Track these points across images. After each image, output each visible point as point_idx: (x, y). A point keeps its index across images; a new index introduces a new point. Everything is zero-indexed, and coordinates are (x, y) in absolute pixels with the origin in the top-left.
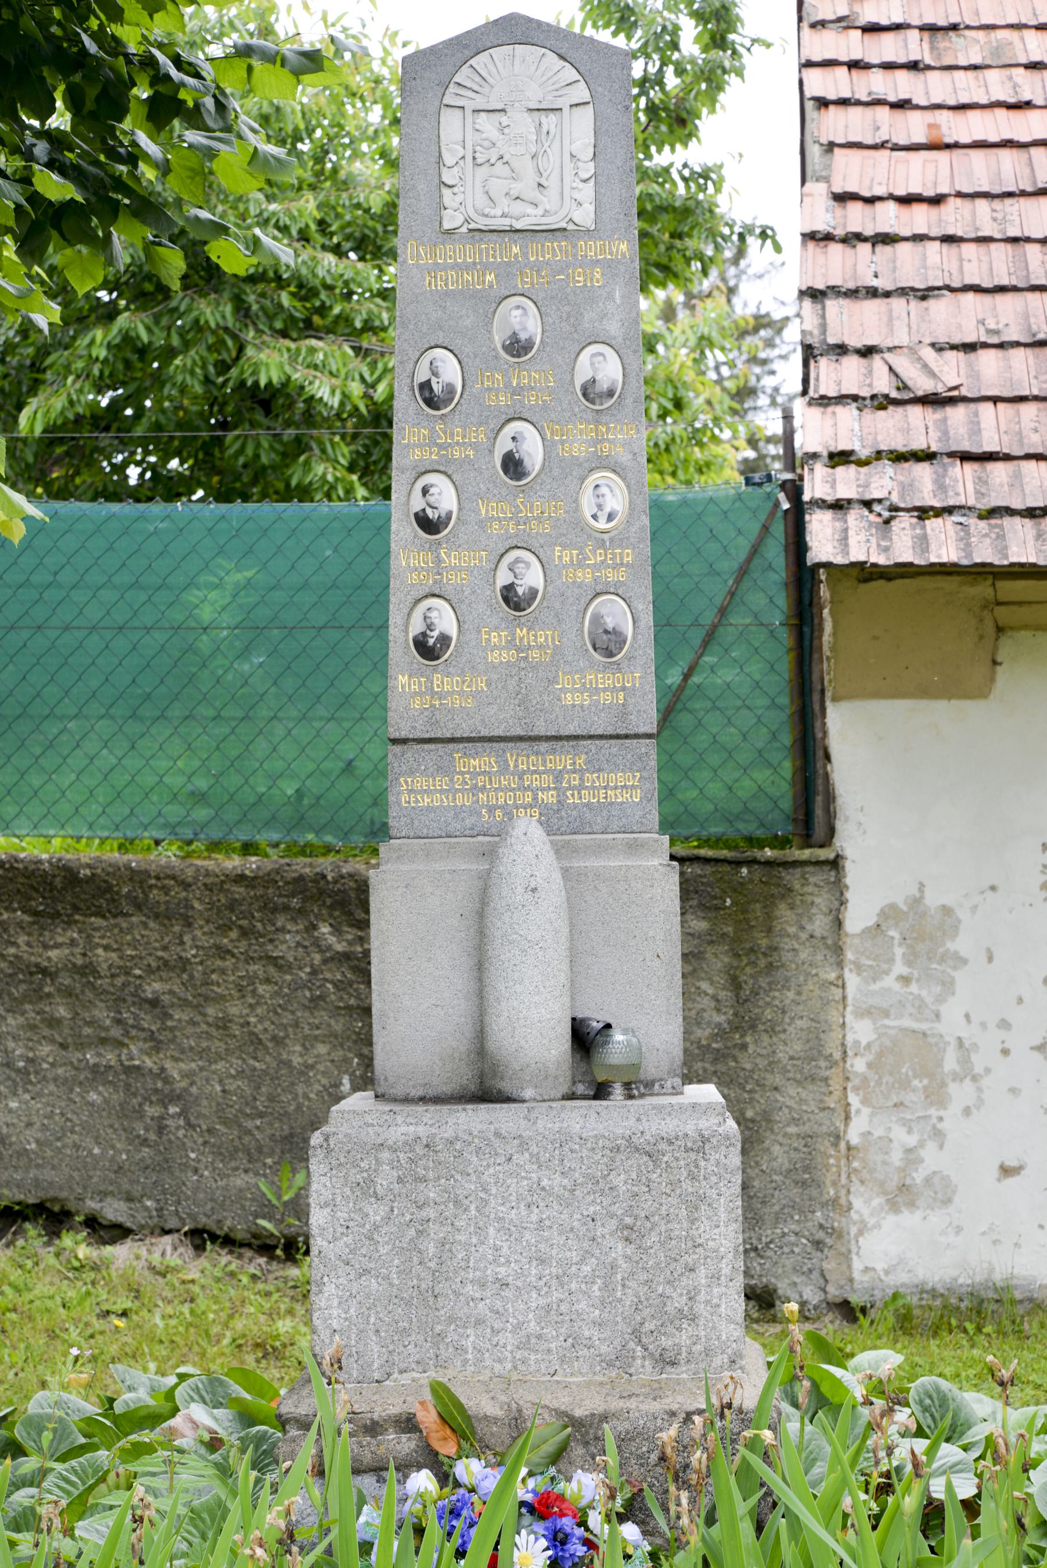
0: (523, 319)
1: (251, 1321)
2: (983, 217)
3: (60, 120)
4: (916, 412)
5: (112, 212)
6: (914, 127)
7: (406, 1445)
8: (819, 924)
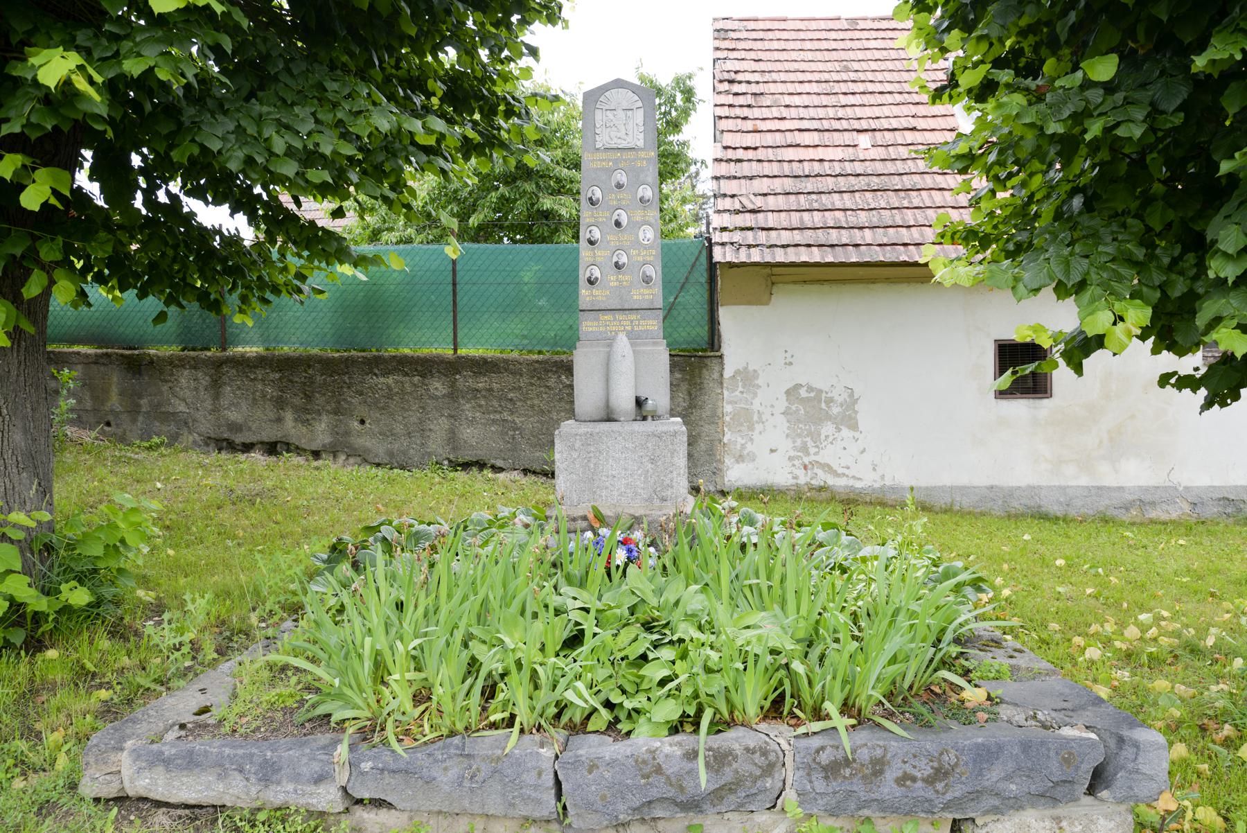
0: (622, 177)
1: (541, 496)
2: (770, 154)
3: (477, 116)
4: (748, 215)
5: (492, 146)
6: (749, 125)
7: (581, 524)
8: (716, 376)
